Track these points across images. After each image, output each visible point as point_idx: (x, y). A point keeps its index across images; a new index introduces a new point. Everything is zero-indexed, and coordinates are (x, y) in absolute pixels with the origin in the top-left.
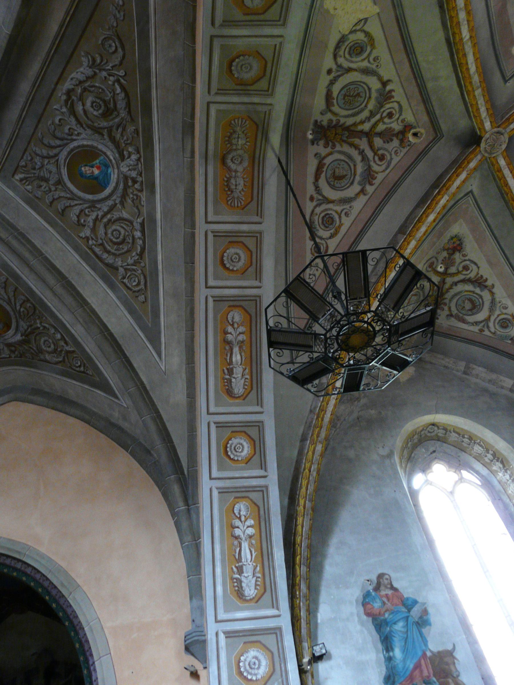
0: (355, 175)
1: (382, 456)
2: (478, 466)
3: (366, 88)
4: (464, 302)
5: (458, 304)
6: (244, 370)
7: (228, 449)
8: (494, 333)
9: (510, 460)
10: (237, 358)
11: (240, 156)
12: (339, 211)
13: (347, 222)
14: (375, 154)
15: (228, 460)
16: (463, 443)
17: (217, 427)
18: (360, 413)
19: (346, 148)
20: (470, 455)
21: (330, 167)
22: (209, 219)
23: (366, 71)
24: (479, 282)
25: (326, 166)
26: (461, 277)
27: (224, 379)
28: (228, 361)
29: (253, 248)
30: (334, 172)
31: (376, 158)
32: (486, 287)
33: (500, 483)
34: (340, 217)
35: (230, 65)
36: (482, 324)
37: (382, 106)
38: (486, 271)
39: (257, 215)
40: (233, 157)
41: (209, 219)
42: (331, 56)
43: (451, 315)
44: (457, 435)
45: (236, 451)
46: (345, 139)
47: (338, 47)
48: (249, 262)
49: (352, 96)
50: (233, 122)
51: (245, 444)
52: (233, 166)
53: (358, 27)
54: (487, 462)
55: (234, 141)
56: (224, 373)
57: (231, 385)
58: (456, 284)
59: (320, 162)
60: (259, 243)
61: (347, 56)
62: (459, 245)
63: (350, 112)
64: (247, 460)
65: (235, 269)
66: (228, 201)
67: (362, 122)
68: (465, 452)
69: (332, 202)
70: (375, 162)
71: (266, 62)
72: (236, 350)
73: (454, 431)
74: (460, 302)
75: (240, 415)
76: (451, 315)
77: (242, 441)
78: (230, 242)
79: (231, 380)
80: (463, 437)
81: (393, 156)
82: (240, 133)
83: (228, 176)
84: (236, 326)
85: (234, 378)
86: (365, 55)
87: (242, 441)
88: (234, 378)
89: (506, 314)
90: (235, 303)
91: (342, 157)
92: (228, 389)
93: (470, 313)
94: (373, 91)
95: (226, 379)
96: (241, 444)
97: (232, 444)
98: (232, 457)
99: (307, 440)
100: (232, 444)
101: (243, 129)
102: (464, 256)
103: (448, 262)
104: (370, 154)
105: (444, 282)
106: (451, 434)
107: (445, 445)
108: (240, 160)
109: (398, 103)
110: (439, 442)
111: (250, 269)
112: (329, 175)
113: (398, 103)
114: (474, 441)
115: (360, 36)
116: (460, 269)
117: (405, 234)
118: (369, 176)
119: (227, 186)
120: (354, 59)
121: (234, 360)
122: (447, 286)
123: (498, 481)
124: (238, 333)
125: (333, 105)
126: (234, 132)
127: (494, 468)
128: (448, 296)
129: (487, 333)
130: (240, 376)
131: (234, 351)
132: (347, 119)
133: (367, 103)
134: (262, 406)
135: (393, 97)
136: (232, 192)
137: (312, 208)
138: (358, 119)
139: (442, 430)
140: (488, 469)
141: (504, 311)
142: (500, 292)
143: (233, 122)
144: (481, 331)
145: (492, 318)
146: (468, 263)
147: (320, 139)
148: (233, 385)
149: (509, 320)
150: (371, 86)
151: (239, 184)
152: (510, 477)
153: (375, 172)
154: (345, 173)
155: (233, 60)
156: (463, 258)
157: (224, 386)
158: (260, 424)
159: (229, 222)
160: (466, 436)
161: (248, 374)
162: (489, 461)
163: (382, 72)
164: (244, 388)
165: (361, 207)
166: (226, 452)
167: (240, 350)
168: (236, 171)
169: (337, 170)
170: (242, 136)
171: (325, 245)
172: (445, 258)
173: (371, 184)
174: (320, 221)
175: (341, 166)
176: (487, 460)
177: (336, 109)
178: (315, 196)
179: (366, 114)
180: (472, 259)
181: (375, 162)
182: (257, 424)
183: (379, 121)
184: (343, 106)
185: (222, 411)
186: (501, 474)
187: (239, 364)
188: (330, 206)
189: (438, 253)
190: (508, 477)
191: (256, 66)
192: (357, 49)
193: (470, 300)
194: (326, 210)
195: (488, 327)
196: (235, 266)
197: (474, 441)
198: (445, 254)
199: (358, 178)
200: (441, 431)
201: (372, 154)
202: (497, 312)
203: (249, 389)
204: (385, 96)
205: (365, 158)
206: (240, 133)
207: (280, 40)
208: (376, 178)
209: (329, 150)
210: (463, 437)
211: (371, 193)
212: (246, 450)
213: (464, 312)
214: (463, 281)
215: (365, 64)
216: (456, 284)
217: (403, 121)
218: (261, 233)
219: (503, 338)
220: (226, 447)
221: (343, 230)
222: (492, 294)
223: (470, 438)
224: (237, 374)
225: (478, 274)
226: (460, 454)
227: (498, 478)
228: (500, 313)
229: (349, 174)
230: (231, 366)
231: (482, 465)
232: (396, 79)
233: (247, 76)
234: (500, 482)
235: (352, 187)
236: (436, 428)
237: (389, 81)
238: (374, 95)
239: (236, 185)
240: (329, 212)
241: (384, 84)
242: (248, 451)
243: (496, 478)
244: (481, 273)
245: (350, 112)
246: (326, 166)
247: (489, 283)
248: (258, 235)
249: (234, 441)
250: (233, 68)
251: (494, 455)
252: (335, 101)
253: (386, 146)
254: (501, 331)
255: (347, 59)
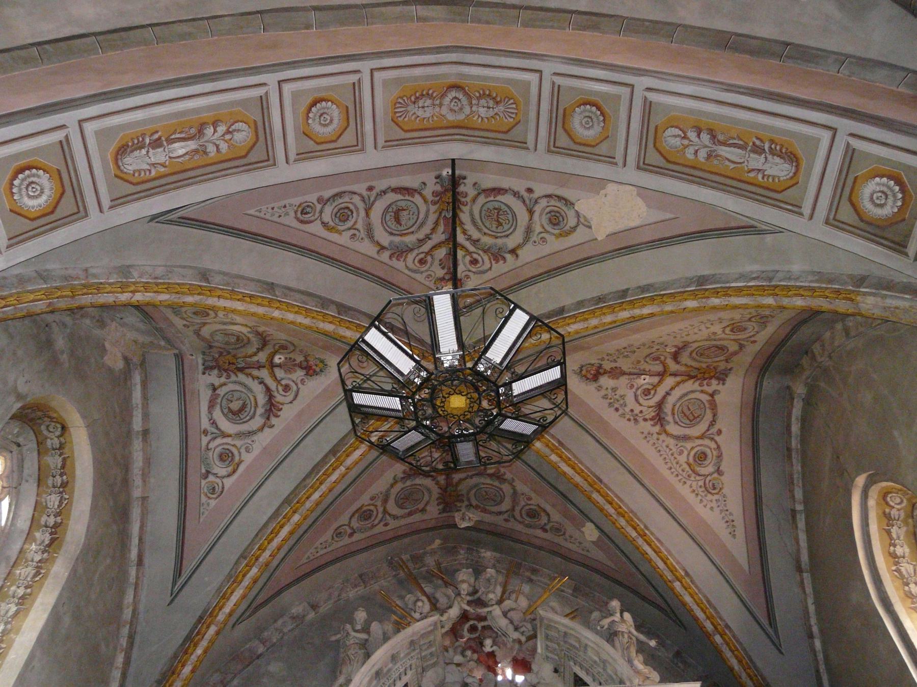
0: (401, 235)
1: (16, 387)
2: (27, 512)
3: (508, 233)
4: (238, 399)
5: (235, 393)
6: (163, 165)
7: (27, 172)
8: (208, 449)
9: (64, 548)
10: (180, 149)
11: (461, 109)
12: (356, 226)
13: (344, 239)
14: (427, 253)
15: (8, 176)
16: (51, 478)
17: (61, 142)
18: (54, 325)
19: (432, 218)
20: (37, 495)
21: (409, 203)
22: (376, 74)
23: (529, 231)
24: (272, 409)
25: (411, 199)
26: (272, 385)
27: (143, 135)
28: (173, 137)
29: (341, 142)
30: (404, 210)
31: (422, 256)
32: (268, 419)
33: (20, 552)
34: (349, 229)
35: (592, 104)
36: (216, 431)
37: (485, 251)
38: (288, 413)
39: (386, 141)
40: (459, 100)
41: (377, 75)
42: (549, 192)
43: (215, 389)
44: (59, 465)
45: (27, 188)
46: (443, 215)
47: (560, 198)
48: (323, 140)
49: (499, 217)
50: (512, 101)
51: (44, 198)
52: (447, 100)
53: (582, 220)
54: (39, 520)
55: (483, 102)
56: (152, 134)
57: (136, 149)
58: (262, 382)
59: (416, 190)
60: (349, 149)
61: (548, 209)
62: (315, 371)
63: (477, 217)
64: (17, 210)
65: (310, 121)
66: (402, 98)
67: (464, 232)
68: (38, 486)
69: (367, 215)
70: (418, 255)
71: (593, 146)
72: (192, 145)
73: (64, 460)
74: (236, 395)
75: (89, 176)
76: (215, 389)
77: (47, 192)
78: (347, 107)
79: (142, 147)
80: (61, 475)
81: (425, 274)
82: (496, 110)
83: (435, 95)
84: (228, 137)
85: (148, 152)
86: (549, 228)
87: (47, 192)
88: (148, 152)
89: (240, 453)
90: (262, 131)
91: (422, 216)
92: (128, 146)
93: (226, 411)
94: (505, 240)
95: (143, 139)
96: (42, 192)
97: (39, 176)
98: (16, 182)
99: (45, 282)
100: (39, 176)
101: (501, 115)
102: (303, 381)
103: (289, 366)
104: (426, 248)
105: (260, 367)
106: (57, 457)
107: (35, 454)
108: (456, 109)
109: (490, 268)
110: (35, 446)
111: (312, 142)
112: (399, 203)
113: (490, 268)
114: (64, 491)
115: (572, 222)
116: (283, 382)
117: (339, 314)
118: (400, 252)
119: (422, 95)
120: (544, 217)
121: (176, 145)
122: (255, 372)
123: (22, 548)
124: (218, 143)
125: (486, 197)
126: (497, 103)
127: (38, 535)
128: (242, 377)
129: (205, 440)
130: (153, 160)
131: (189, 143)
132: (468, 214)
133: (489, 235)
134: (111, 207)
135: (497, 262)
136: (414, 103)
137: (359, 191)
138: (469, 226)
139: (58, 442)
140: (30, 527)
141: (243, 450)
142: (265, 438)
143: (512, 101)
144: (205, 432)
145: (228, 440)
146: (295, 388)
147: (442, 186)
148: (137, 153)
149: (232, 460)
150: (510, 237)
151: (425, 112)
152: (40, 561)
153: (406, 257)
154: (403, 223)
155: (599, 108)
156: (299, 382)
157: (132, 139)
158: (82, 213)
159: (376, 102)
160: (65, 477)
161: (157, 171)
162: (43, 523)
163: (529, 247)
164: (134, 171)
165: (363, 252)
166: (21, 170)
167: (193, 151)
168: (441, 105)
169: (405, 213)
170: (491, 113)
171: (313, 218)
172: (295, 360)
173: (390, 257)
174: (343, 206)
175: (411, 216)
176: (43, 520)
177: (482, 199)
178: (374, 193)
179: (476, 235)
180: (300, 392)
181: (418, 255)
182: (81, 209)
183: (467, 250)
184: (484, 208)
185: (89, 146)
186: (34, 547)
187: (172, 155)
188: (362, 213)
189: (301, 351)
190: (38, 558)
191: (589, 134)
192: (555, 219)
193: (244, 407)
194: (357, 209)
195: (215, 438)
196: (314, 120)
197: (64, 491)
198: (300, 359)
199: (397, 239)
200: (56, 442)
201: (426, 250)
202: (238, 443)
203: (135, 181)
204: (497, 255)
205: (421, 242)
206: (496, 110)
207: (621, 164)
208: (398, 260)
209: (430, 198)
210: (61, 475)
211: (381, 259)
212: (34, 204)
213: (224, 402)
214: (268, 389)
215: (538, 229)
216: (262, 382)
217: (468, 277)
218: (362, 150)
219: (204, 460)
220: (29, 168)
221: (334, 237)
222: (261, 429)
223: (64, 485)
224: (154, 154)
225: (282, 404)
226: (31, 481)
227: (26, 546)
228: (239, 446)
229: (402, 228)
230: (165, 143)
231: (30, 516)
232: (519, 263)
233: (576, 123)
234: (21, 551)
235: (387, 234)
236: (58, 433)
237: (517, 256)
238: (499, 242)
239: (423, 107)
240: (355, 215)
241: (513, 252)
242: (33, 207)
243: (24, 543)
244: (285, 408)
245: (477, 217)
246: (411, 199)
247: (274, 421)
248: (360, 147)
249: (44, 179)
250: (588, 107)
251: (56, 526)
252: (492, 198)
253: (437, 262)
254: (214, 456)
255: (544, 209)
